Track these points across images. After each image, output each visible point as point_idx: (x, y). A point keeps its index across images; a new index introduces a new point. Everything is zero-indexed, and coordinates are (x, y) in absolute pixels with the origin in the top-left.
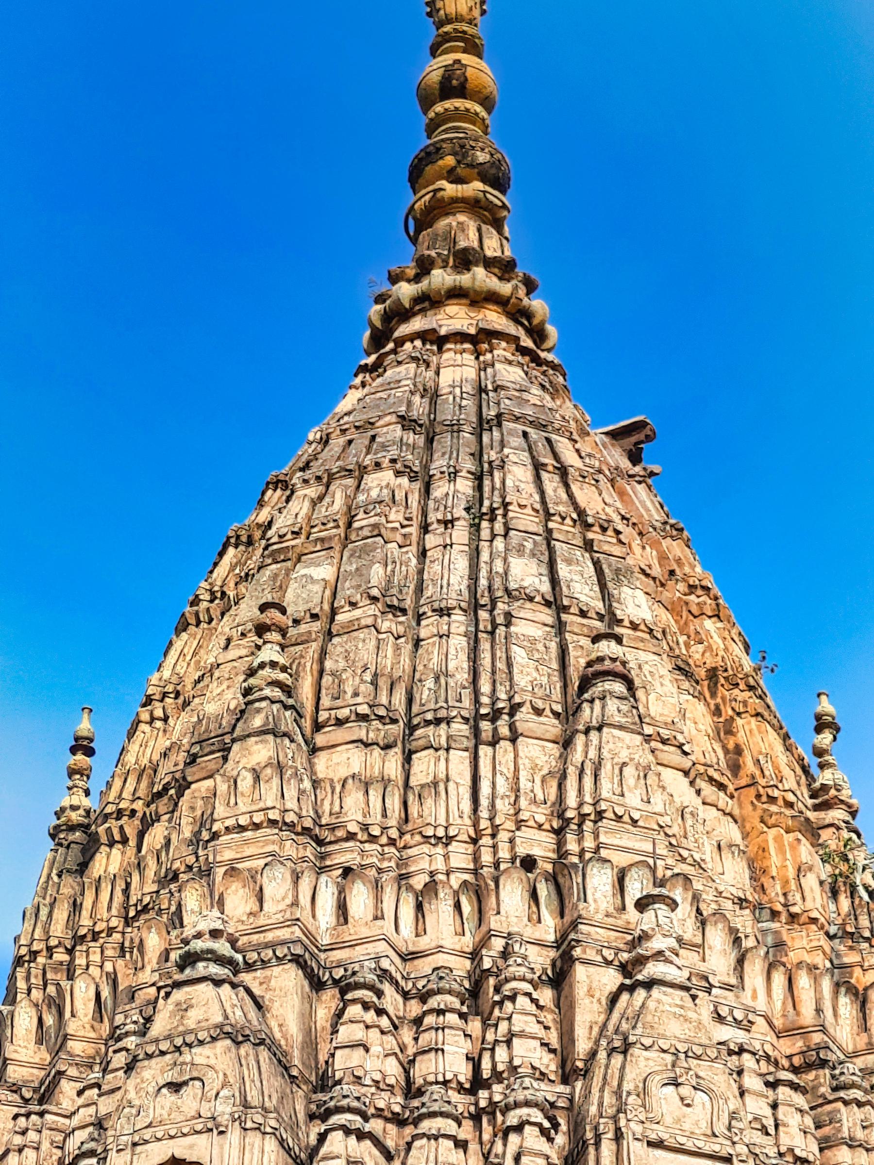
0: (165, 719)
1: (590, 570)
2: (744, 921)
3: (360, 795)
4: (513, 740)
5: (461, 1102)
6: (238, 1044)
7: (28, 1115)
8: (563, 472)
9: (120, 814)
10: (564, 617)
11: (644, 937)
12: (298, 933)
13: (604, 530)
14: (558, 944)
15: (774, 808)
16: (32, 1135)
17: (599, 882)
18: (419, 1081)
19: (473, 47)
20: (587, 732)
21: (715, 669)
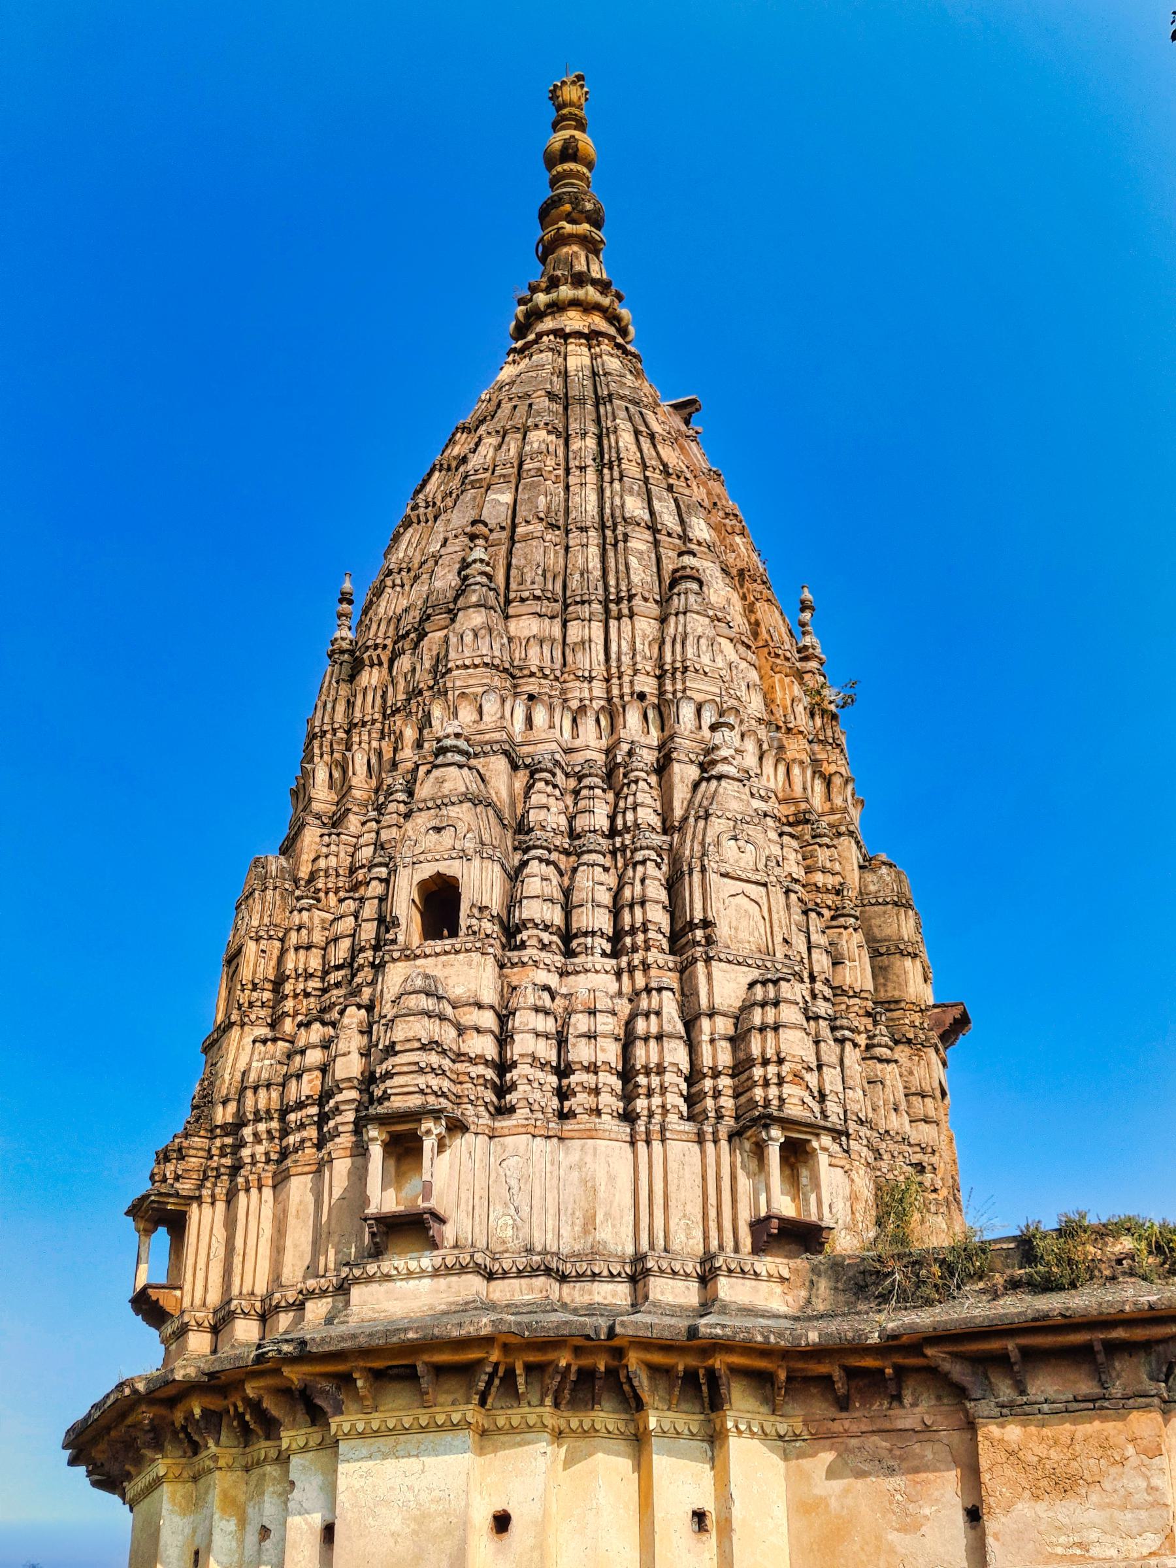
0: (402, 586)
1: (673, 505)
2: (762, 732)
3: (538, 648)
4: (631, 617)
5: (605, 843)
6: (475, 805)
7: (330, 835)
8: (652, 436)
9: (376, 646)
10: (658, 536)
11: (716, 748)
12: (505, 737)
13: (679, 477)
14: (660, 748)
15: (778, 661)
16: (333, 848)
17: (687, 711)
18: (579, 830)
19: (581, 126)
20: (677, 614)
21: (742, 570)
